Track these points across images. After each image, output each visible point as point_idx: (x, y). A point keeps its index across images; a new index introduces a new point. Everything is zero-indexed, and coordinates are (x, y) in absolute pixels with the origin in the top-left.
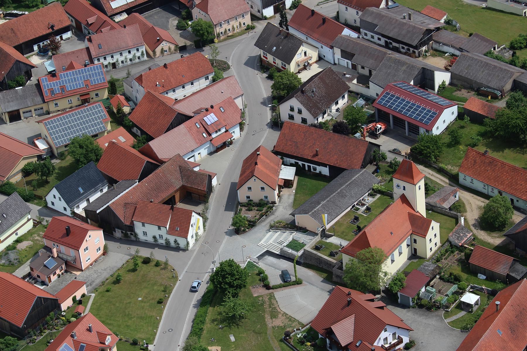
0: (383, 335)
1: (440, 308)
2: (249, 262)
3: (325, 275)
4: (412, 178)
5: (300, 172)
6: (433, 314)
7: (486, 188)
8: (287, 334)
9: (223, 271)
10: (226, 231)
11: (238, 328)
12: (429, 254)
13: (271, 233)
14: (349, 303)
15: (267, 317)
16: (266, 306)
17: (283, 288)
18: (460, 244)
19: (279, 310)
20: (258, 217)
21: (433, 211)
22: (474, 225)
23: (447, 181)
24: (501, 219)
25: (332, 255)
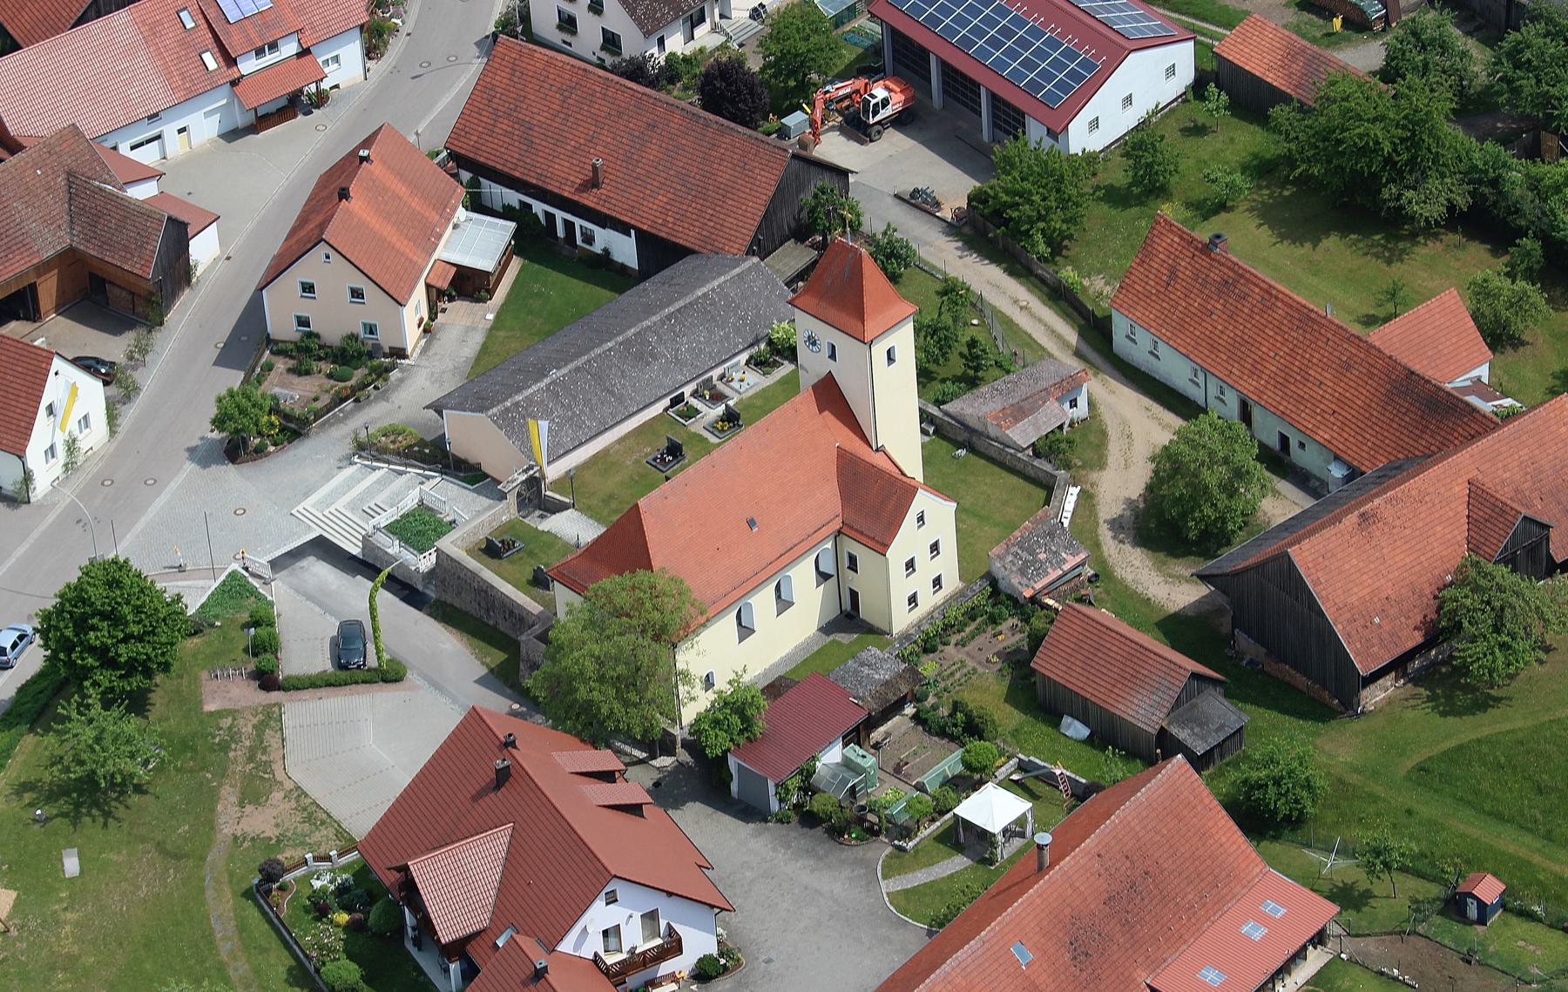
0: (599, 916)
1: (877, 834)
2: (233, 575)
3: (498, 657)
4: (859, 314)
5: (532, 241)
6: (848, 854)
7: (1201, 380)
8: (271, 874)
9: (84, 601)
10: (195, 442)
11: (105, 825)
12: (902, 620)
13: (352, 469)
14: (503, 777)
15: (228, 795)
16: (237, 753)
17: (323, 692)
18: (1028, 593)
19: (280, 775)
20: (326, 400)
21: (972, 449)
22: (1116, 525)
23: (1072, 337)
24: (1208, 511)
25: (539, 581)
